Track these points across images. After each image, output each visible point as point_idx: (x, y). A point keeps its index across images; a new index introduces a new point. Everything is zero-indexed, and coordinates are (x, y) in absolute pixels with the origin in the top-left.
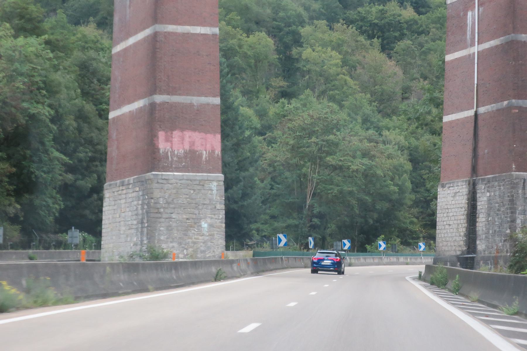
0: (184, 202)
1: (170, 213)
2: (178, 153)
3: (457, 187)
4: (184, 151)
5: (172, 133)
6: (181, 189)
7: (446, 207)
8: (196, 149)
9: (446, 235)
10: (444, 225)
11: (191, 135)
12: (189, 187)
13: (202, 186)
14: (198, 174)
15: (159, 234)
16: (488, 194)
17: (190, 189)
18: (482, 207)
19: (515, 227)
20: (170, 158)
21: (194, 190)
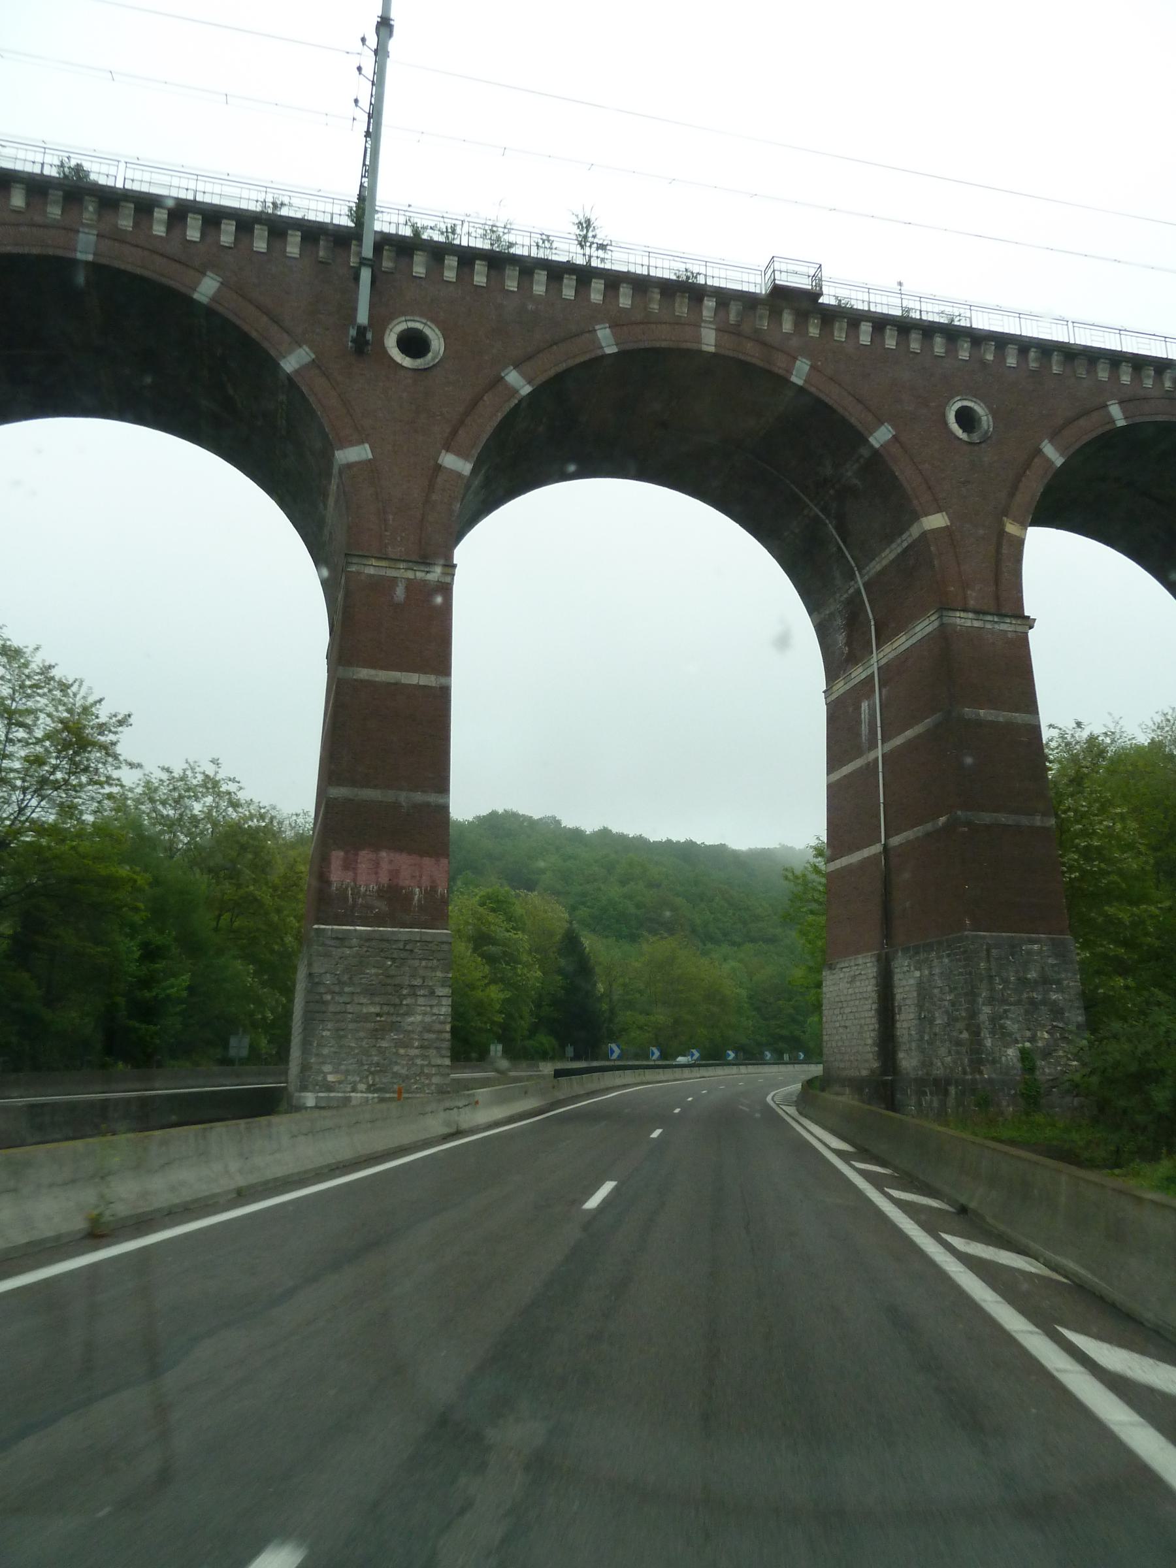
0: (374, 982)
1: (343, 1003)
2: (366, 890)
3: (856, 968)
4: (379, 888)
5: (357, 855)
6: (369, 957)
7: (837, 999)
8: (401, 883)
9: (840, 1044)
10: (835, 1028)
11: (393, 859)
12: (382, 954)
13: (409, 952)
14: (402, 930)
15: (319, 1045)
16: (917, 974)
17: (387, 958)
18: (905, 996)
19: (978, 1026)
20: (350, 900)
21: (394, 960)
